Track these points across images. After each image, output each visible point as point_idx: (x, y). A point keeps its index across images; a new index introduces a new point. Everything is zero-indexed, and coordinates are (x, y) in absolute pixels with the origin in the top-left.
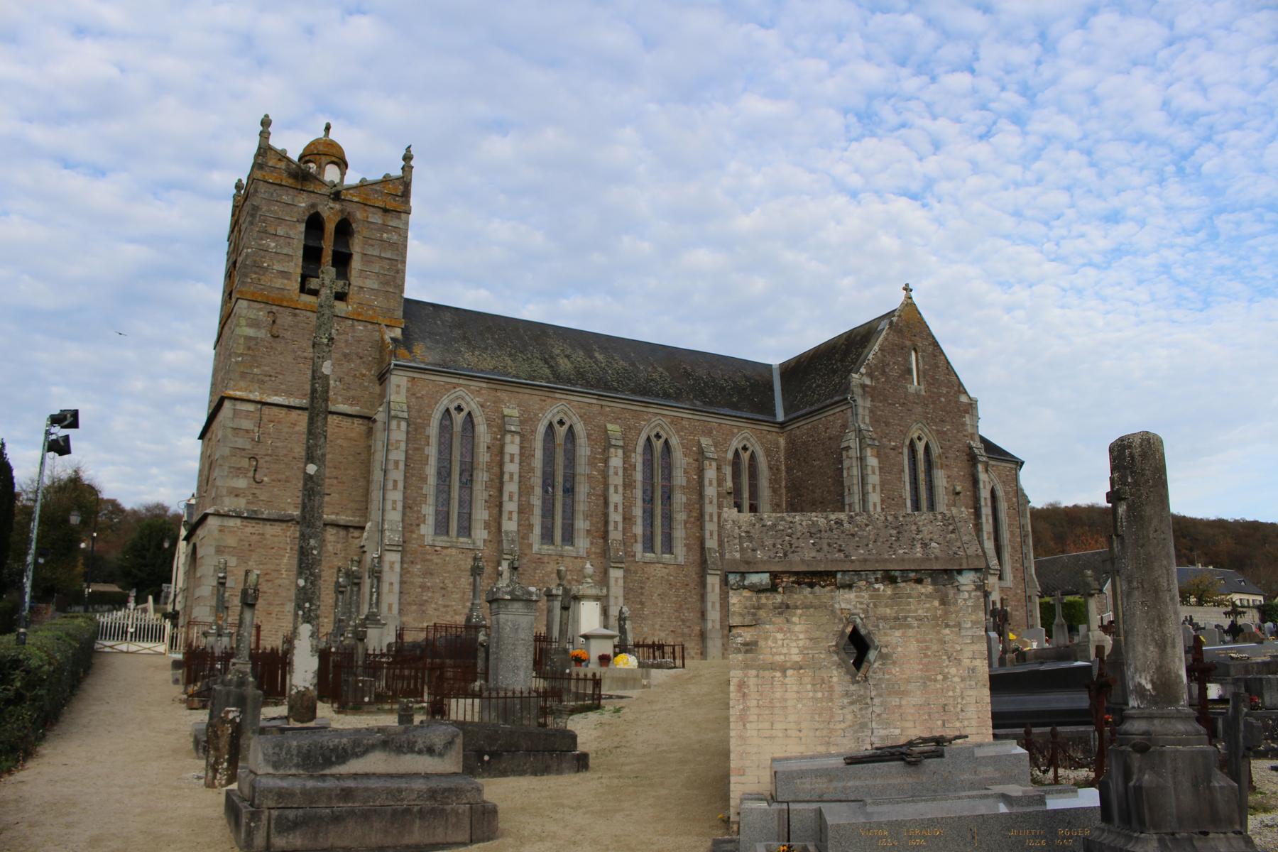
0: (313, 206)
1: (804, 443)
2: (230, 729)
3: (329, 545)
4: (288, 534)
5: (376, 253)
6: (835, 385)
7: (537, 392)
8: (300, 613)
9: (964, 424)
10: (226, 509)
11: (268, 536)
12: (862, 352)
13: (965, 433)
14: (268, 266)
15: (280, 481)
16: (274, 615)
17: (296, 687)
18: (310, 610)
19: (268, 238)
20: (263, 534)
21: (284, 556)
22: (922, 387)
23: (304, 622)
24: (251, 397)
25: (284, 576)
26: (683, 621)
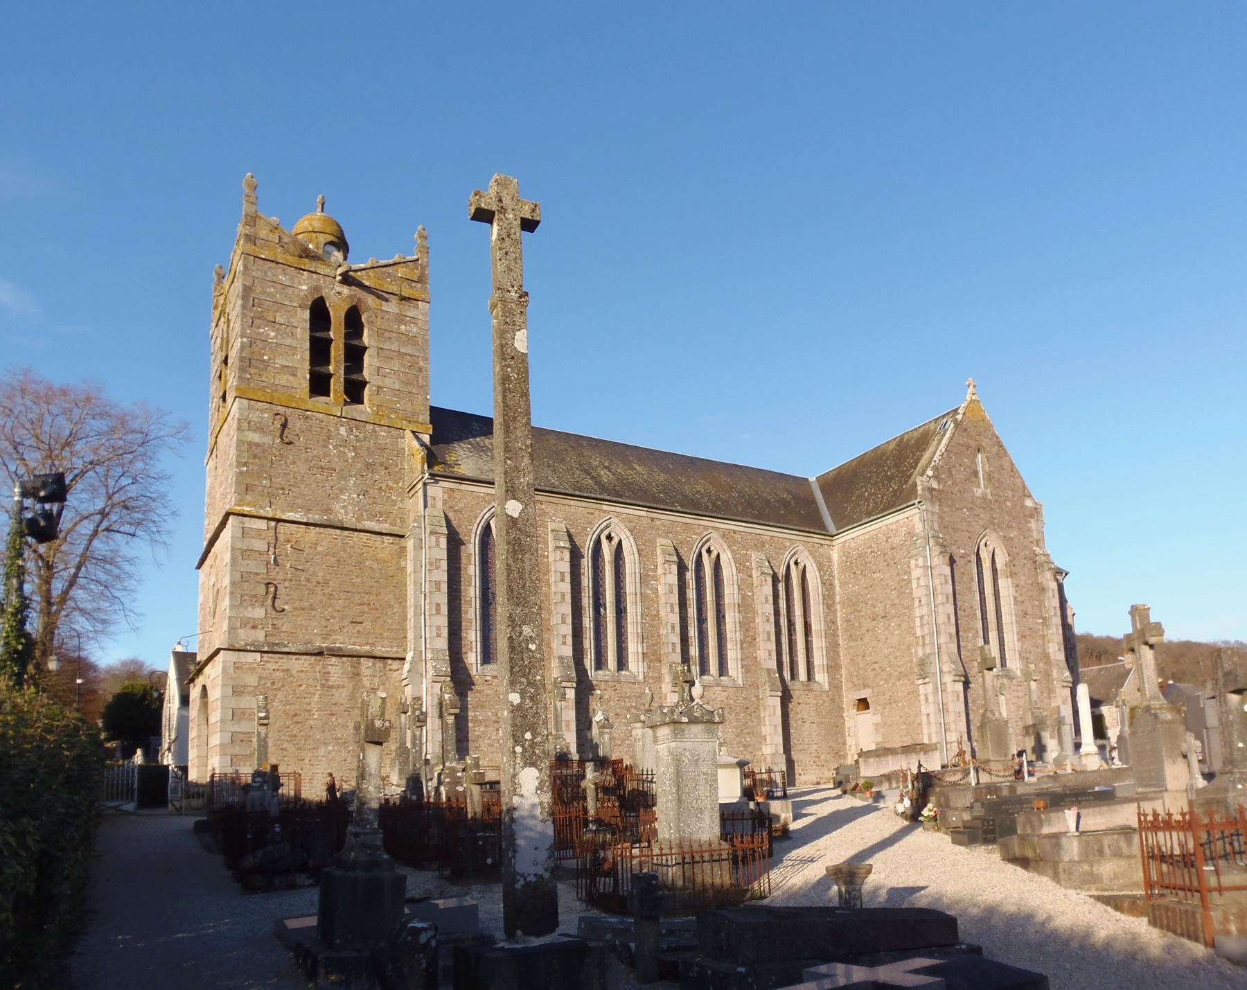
0: (317, 289)
1: (860, 555)
2: (424, 961)
3: (364, 679)
4: (318, 668)
5: (394, 347)
6: (895, 492)
7: (584, 504)
8: (519, 749)
9: (1030, 530)
10: (242, 643)
11: (294, 672)
12: (922, 456)
13: (1031, 539)
14: (270, 359)
15: (303, 609)
16: (307, 761)
17: (522, 875)
18: (533, 744)
19: (266, 326)
20: (288, 670)
21: (314, 694)
22: (988, 491)
23: (526, 765)
24: (262, 513)
25: (316, 716)
26: (745, 746)
